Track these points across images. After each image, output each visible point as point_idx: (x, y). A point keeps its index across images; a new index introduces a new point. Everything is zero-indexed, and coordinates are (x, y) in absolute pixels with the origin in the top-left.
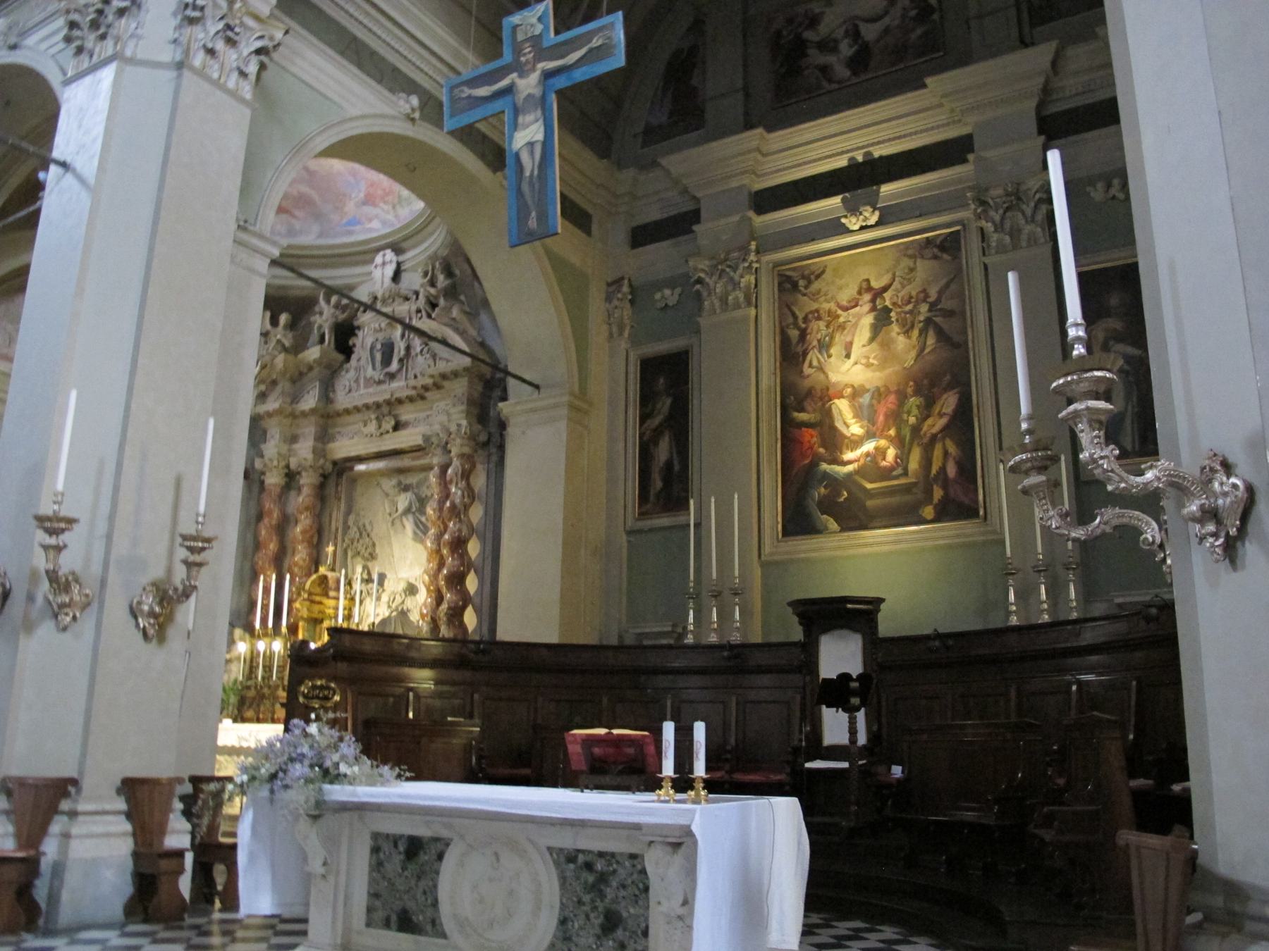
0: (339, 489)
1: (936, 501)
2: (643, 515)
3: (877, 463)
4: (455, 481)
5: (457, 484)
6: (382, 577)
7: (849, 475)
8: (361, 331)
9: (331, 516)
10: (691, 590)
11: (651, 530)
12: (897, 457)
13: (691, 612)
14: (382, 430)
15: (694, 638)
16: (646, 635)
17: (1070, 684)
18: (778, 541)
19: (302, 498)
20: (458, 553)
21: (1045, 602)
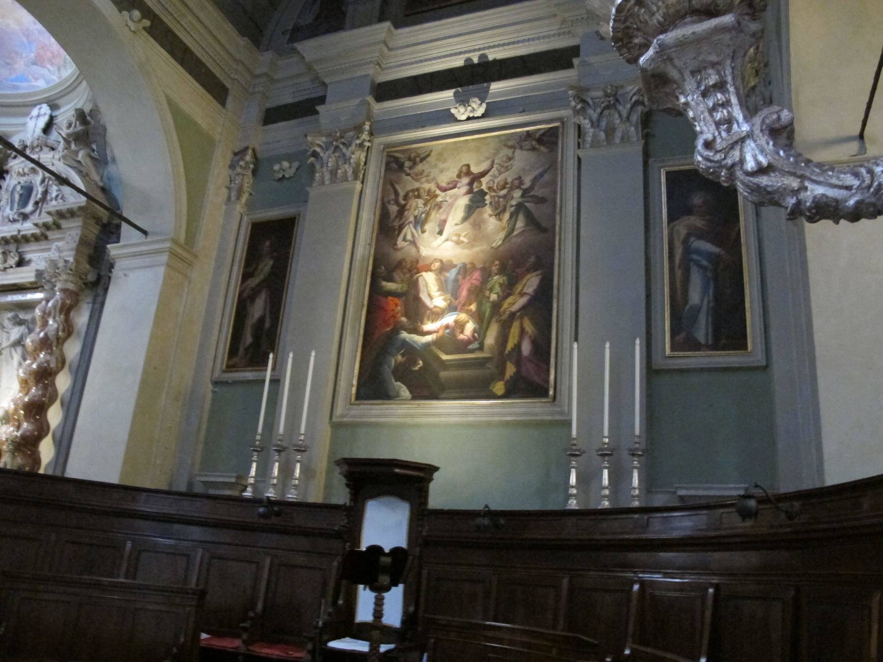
2: (230, 368)
3: (455, 336)
4: (53, 314)
7: (427, 345)
11: (235, 383)
12: (475, 331)
14: (7, 265)
15: (253, 492)
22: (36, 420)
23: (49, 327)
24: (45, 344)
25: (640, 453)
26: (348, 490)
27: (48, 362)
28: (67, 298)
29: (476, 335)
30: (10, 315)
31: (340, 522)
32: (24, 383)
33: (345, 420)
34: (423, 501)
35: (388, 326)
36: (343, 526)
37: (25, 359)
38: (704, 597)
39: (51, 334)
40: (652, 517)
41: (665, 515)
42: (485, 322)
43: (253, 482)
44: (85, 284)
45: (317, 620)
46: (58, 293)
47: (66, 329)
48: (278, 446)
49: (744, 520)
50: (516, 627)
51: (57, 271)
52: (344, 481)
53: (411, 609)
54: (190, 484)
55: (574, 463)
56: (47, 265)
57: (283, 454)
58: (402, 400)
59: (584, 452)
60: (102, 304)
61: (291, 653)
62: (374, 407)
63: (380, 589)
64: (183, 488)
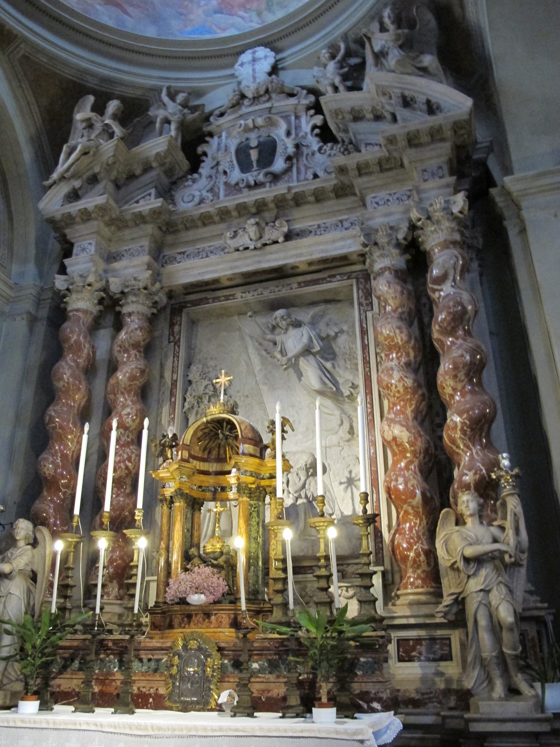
0: (176, 328)
8: (216, 138)
9: (162, 366)
14: (265, 240)
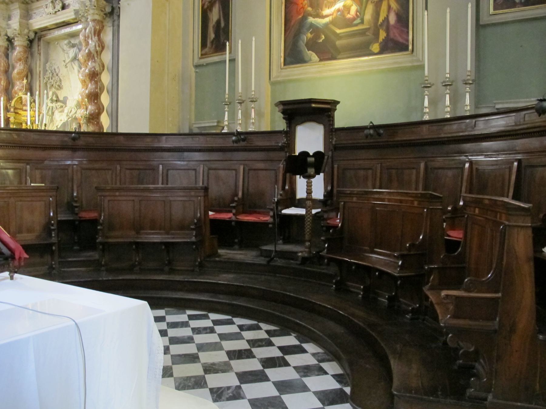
0: (40, 47)
1: (381, 40)
2: (203, 55)
3: (344, 16)
4: (90, 37)
5: (92, 39)
6: (66, 98)
7: (326, 25)
10: (227, 100)
11: (208, 65)
12: (357, 11)
13: (227, 113)
14: (56, 10)
15: (228, 129)
16: (204, 128)
17: (464, 163)
18: (281, 69)
19: (18, 52)
20: (95, 81)
21: (449, 106)
22: (96, 103)
23: (90, 45)
24: (90, 56)
25: (471, 82)
26: (285, 121)
27: (94, 67)
28: (96, 25)
29: (358, 13)
30: (66, 42)
31: (281, 141)
32: (84, 82)
33: (279, 79)
34: (331, 123)
35: (300, 14)
36: (284, 143)
37: (81, 68)
38: (510, 169)
39: (92, 50)
40: (478, 121)
41: (487, 118)
42: (364, 5)
43: (227, 124)
44: (105, 14)
45: (274, 198)
46: (90, 23)
47: (100, 45)
48: (239, 100)
49: (540, 115)
50: (392, 191)
51: (86, 8)
52: (282, 115)
53: (329, 188)
54: (190, 129)
55: (427, 92)
56: (80, 6)
57: (242, 104)
58: (314, 62)
59: (433, 85)
60: (119, 26)
61: (261, 218)
62: (295, 69)
63: (309, 177)
64: (187, 131)
